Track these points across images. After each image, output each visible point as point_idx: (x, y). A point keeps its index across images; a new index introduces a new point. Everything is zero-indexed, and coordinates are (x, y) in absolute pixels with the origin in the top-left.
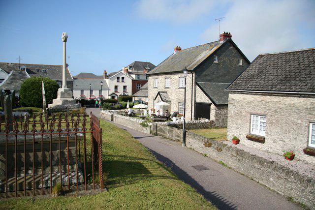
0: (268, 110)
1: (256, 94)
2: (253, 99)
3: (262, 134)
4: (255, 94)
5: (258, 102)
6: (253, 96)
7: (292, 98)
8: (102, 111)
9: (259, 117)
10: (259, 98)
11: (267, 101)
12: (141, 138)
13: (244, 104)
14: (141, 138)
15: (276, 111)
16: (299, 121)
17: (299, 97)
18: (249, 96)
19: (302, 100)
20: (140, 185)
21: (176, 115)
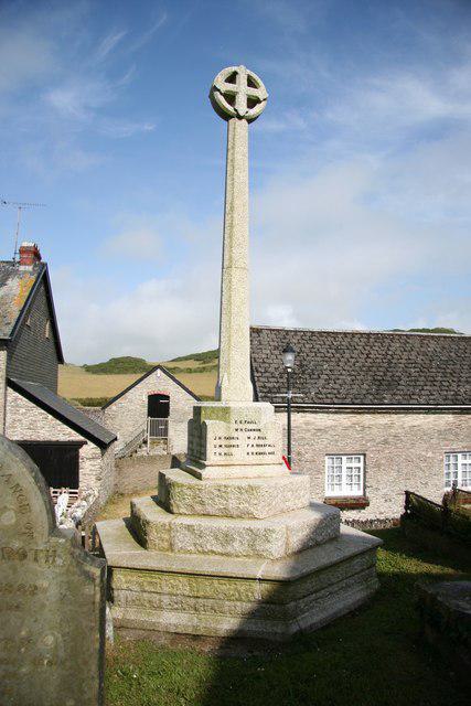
0: (368, 441)
1: (339, 411)
2: (329, 423)
3: (357, 492)
4: (336, 413)
5: (346, 429)
6: (331, 415)
7: (415, 416)
8: (359, 596)
9: (344, 458)
10: (345, 420)
11: (367, 423)
12: (123, 394)
13: (308, 435)
14: (123, 394)
15: (386, 442)
16: (430, 454)
17: (426, 413)
18: (320, 416)
19: (432, 417)
20: (46, 533)
21: (54, 561)
